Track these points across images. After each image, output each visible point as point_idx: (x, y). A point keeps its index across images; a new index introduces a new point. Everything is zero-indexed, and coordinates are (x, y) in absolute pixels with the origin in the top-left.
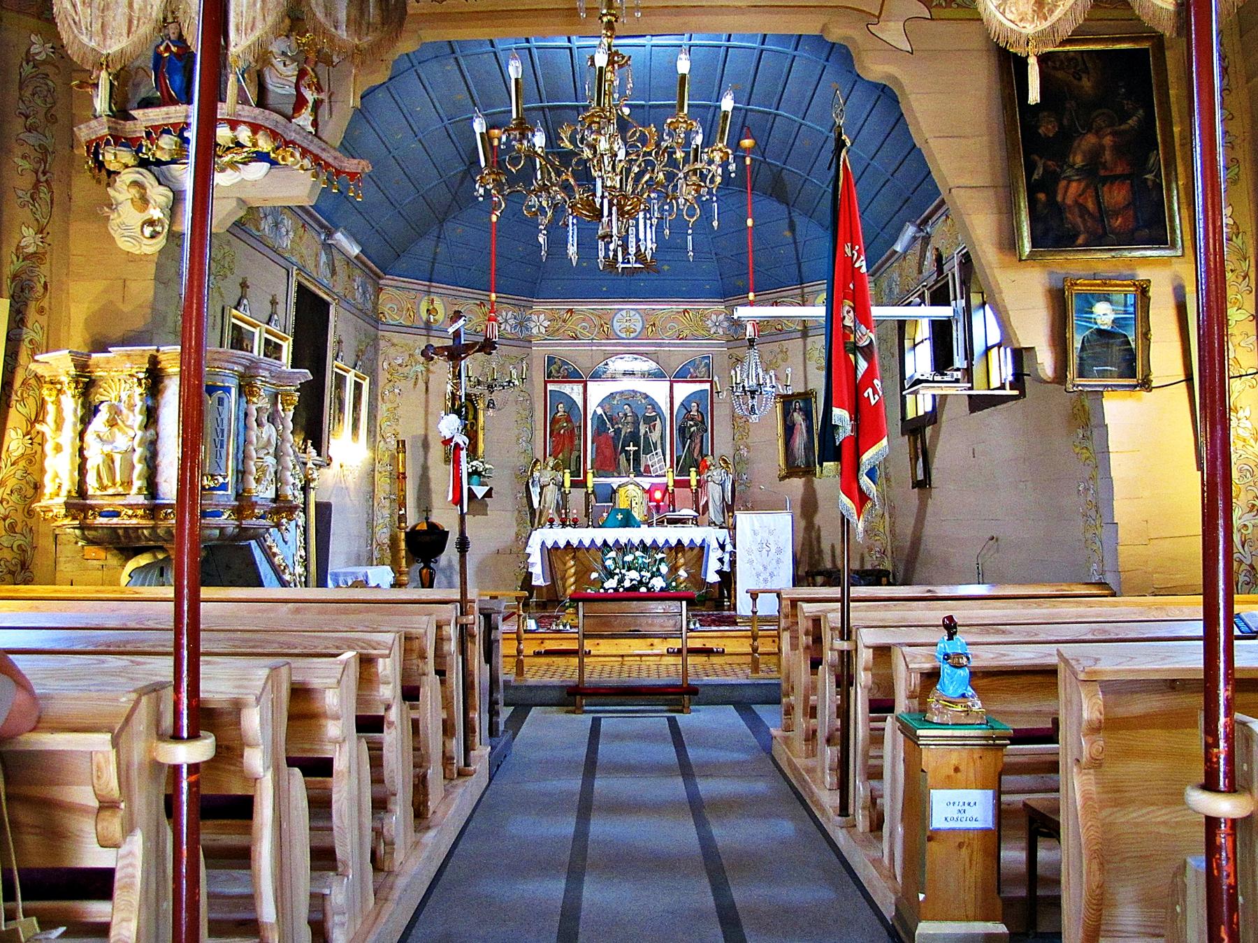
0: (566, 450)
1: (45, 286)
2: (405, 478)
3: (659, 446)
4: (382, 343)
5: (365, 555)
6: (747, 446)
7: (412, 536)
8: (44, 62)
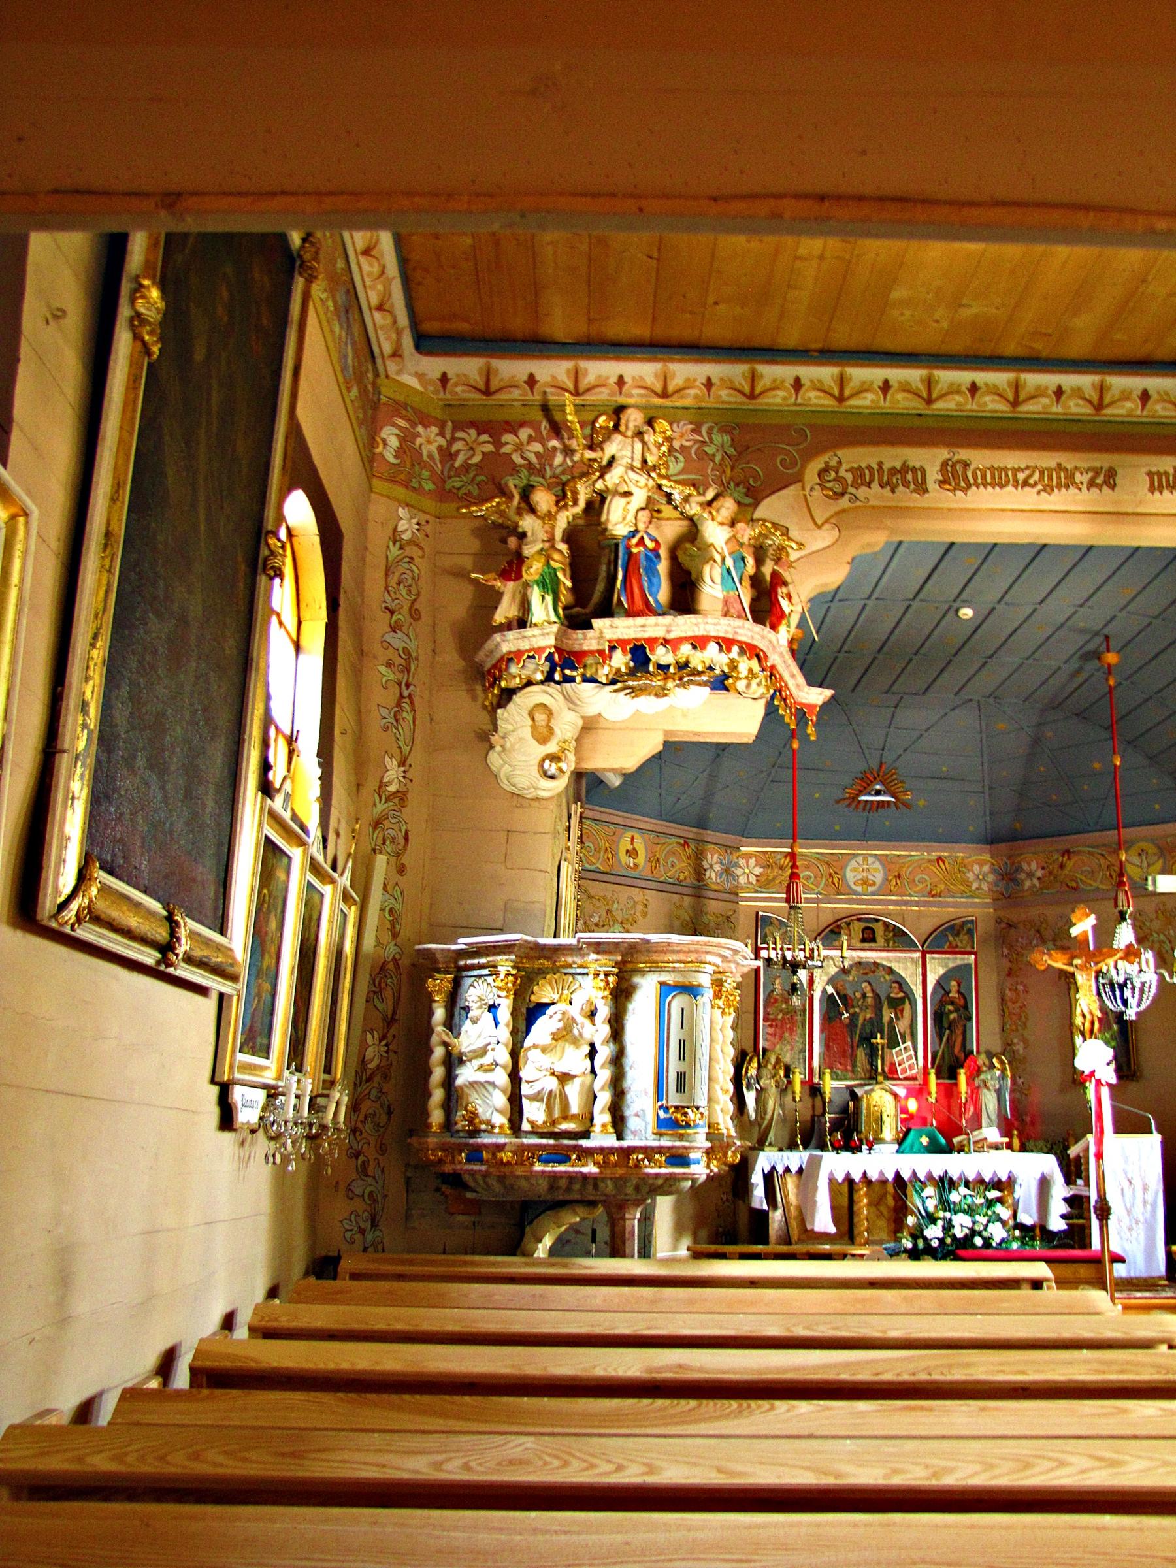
1: (406, 839)
3: (908, 1037)
6: (1025, 1041)
8: (411, 542)
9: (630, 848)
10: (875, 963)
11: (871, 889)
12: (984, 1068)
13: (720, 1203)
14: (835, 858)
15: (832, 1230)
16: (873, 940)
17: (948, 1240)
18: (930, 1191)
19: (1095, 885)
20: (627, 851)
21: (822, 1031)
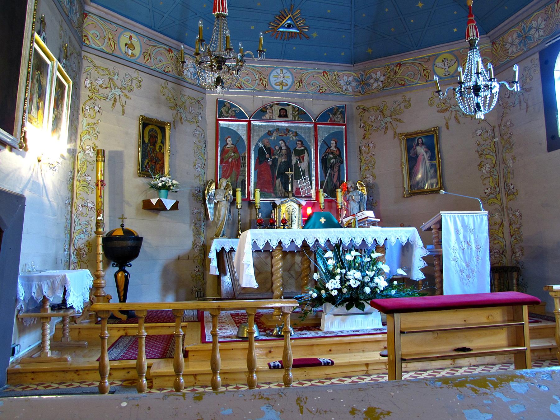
0: (233, 175)
2: (103, 185)
3: (307, 173)
4: (85, 64)
5: (62, 258)
6: (373, 175)
7: (109, 240)
9: (129, 43)
10: (287, 129)
11: (285, 88)
12: (352, 190)
13: (194, 273)
14: (264, 69)
15: (255, 285)
16: (286, 116)
17: (345, 290)
18: (329, 254)
19: (416, 81)
20: (126, 44)
21: (255, 169)
